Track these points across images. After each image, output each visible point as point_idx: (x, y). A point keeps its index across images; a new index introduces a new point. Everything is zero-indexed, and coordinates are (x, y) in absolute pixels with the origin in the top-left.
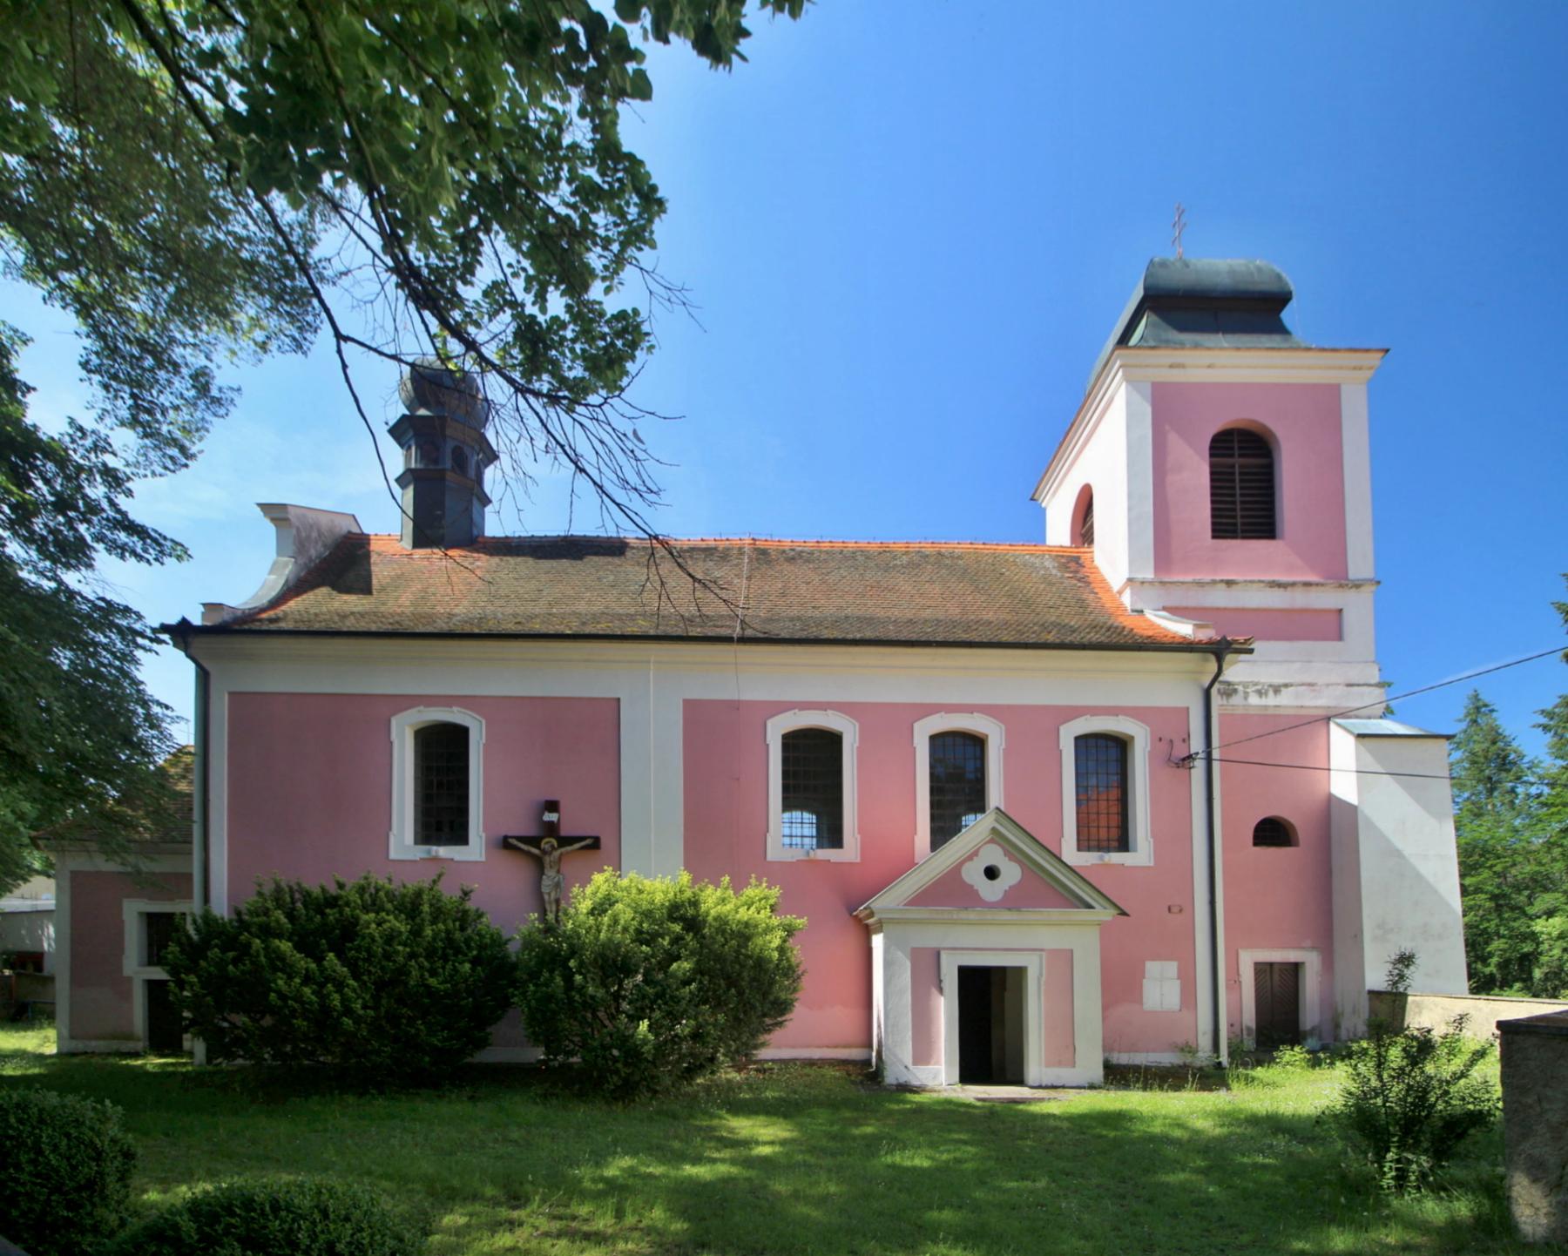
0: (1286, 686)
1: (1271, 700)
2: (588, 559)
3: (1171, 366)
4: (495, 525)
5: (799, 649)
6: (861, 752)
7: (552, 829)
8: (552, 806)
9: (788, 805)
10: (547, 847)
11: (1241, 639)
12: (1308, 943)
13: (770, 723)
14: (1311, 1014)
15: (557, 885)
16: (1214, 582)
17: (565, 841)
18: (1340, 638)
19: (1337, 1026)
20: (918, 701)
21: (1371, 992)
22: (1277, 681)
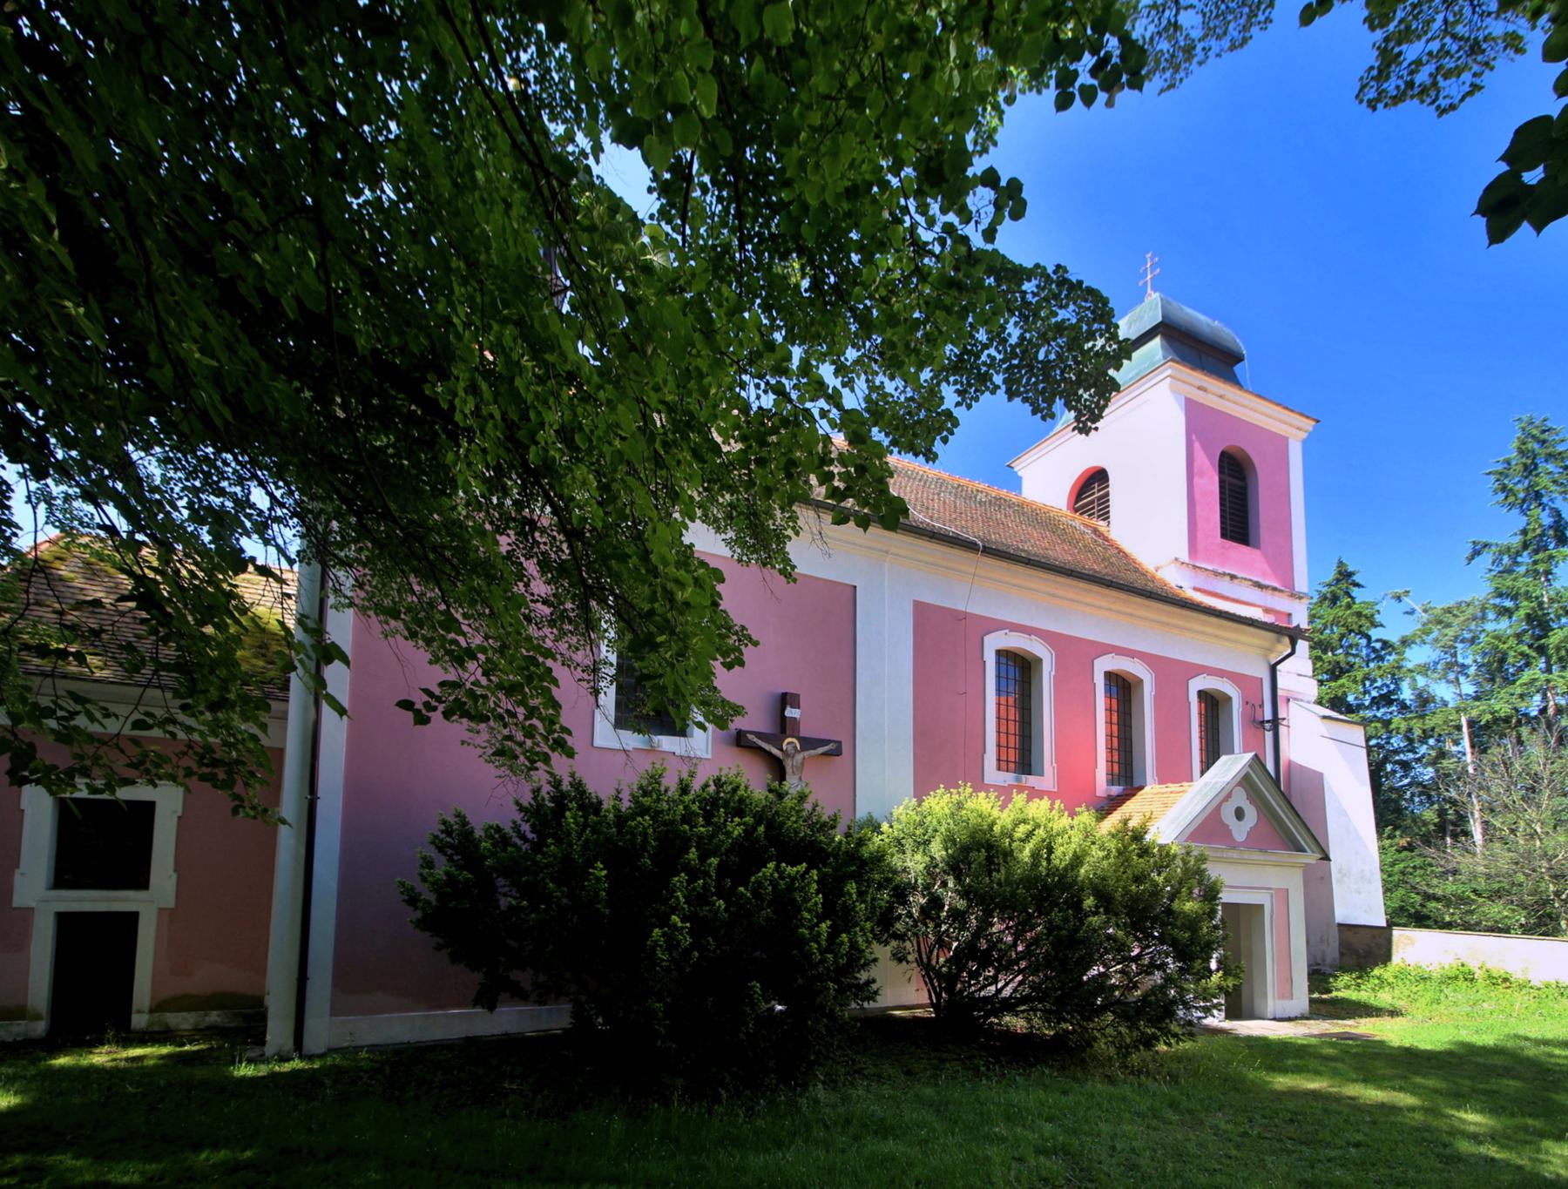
3: (1199, 388)
4: (1157, 342)
5: (1020, 568)
16: (1224, 574)
17: (808, 744)
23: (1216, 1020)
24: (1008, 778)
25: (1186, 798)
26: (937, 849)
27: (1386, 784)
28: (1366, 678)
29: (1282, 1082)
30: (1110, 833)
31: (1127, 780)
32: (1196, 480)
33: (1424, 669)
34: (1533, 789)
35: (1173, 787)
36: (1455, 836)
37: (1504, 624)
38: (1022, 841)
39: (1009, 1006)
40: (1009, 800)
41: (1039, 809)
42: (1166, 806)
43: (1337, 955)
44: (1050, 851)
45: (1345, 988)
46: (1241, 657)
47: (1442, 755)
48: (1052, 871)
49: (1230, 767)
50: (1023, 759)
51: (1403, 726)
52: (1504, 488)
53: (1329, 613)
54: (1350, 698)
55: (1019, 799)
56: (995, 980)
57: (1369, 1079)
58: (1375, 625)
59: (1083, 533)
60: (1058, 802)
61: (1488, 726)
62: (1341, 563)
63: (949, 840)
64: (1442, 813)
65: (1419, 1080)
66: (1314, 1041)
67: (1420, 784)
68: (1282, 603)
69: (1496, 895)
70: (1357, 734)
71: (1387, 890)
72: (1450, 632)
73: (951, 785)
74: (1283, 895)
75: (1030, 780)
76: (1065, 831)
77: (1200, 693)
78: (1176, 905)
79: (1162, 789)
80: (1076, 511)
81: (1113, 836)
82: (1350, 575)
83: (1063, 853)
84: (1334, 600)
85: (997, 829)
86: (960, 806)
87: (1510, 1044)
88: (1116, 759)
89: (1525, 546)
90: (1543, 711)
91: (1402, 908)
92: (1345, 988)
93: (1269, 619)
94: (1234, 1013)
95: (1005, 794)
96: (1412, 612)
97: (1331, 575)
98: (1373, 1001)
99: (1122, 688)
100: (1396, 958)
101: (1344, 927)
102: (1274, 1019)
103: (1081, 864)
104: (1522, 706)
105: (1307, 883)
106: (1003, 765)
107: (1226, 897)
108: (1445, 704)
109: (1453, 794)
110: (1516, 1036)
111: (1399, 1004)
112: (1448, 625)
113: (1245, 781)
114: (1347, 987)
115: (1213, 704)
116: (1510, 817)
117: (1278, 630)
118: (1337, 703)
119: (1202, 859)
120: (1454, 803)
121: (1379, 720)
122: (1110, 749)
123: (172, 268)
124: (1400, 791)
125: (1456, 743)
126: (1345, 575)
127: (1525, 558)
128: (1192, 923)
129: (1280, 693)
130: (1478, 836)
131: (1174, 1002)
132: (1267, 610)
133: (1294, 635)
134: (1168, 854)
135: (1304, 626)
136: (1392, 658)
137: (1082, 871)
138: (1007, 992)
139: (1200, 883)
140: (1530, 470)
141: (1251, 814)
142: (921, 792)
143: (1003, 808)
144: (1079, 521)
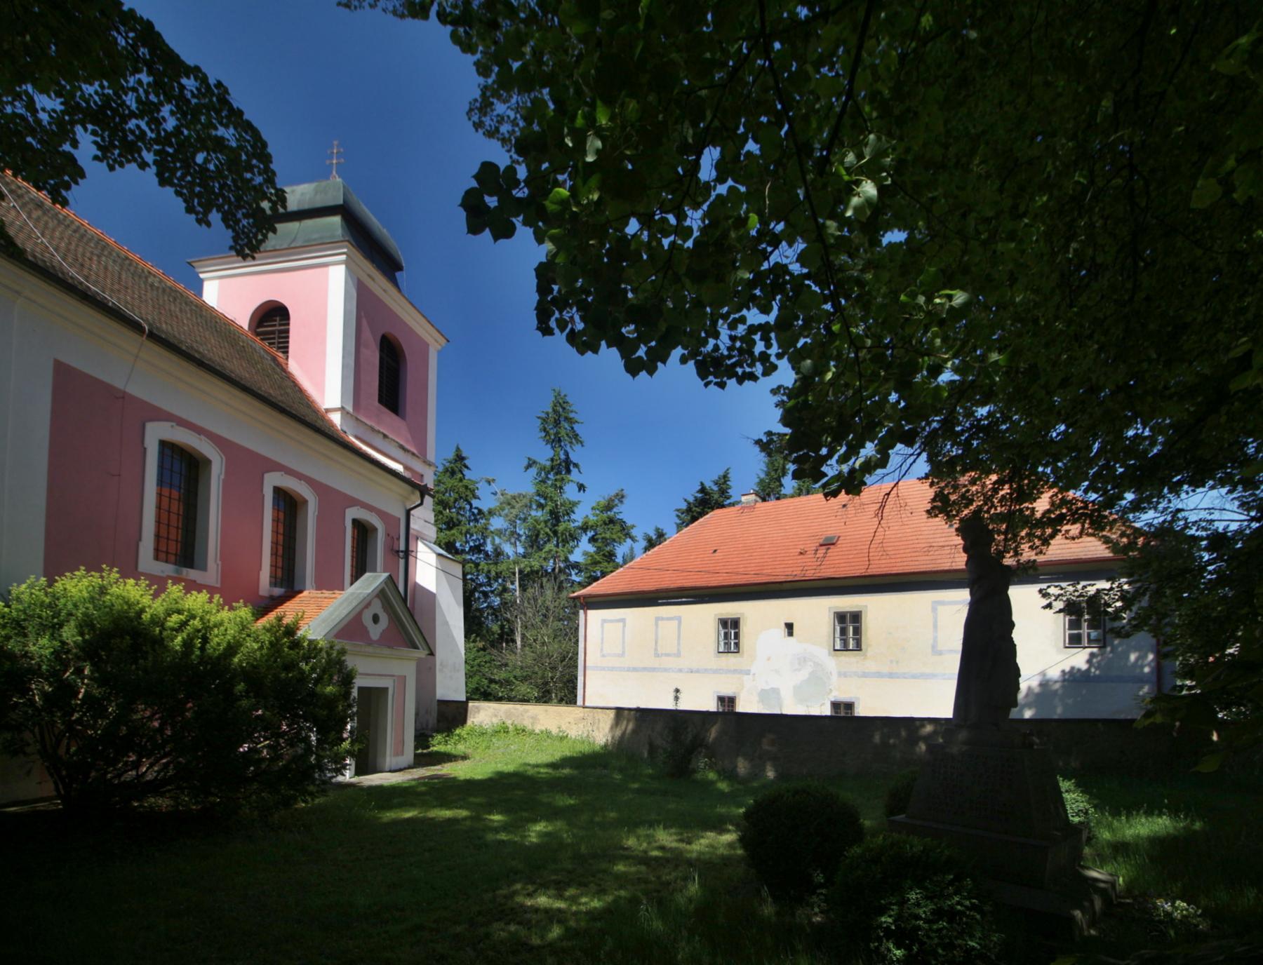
5: (193, 368)
16: (379, 432)
23: (348, 776)
24: (166, 569)
25: (336, 602)
26: (69, 633)
27: (475, 606)
28: (467, 532)
29: (390, 815)
30: (264, 628)
31: (289, 582)
32: (363, 350)
33: (500, 533)
34: (545, 616)
35: (327, 593)
36: (507, 643)
37: (539, 513)
38: (172, 629)
39: (155, 787)
40: (161, 589)
41: (196, 601)
42: (320, 608)
44: (205, 640)
45: (438, 744)
46: (390, 500)
47: (505, 590)
48: (204, 659)
49: (371, 582)
50: (183, 547)
51: (486, 568)
52: (545, 430)
53: (450, 482)
54: (458, 545)
55: (175, 590)
56: (136, 765)
57: (445, 804)
58: (476, 497)
59: (262, 357)
60: (217, 597)
61: (528, 575)
62: (458, 449)
63: (86, 624)
64: (502, 627)
65: (472, 799)
66: (413, 783)
67: (492, 607)
68: (418, 466)
69: (524, 679)
70: (458, 570)
71: (469, 676)
72: (514, 512)
73: (93, 567)
74: (403, 679)
75: (192, 574)
76: (221, 624)
77: (164, 445)
78: (318, 689)
79: (315, 593)
80: (258, 334)
81: (268, 630)
83: (218, 641)
84: (453, 473)
85: (146, 617)
86: (103, 590)
87: (521, 769)
88: (280, 564)
89: (552, 468)
90: (554, 570)
91: (477, 689)
92: (438, 744)
93: (407, 475)
94: (360, 771)
95: (159, 585)
96: (495, 494)
97: (451, 455)
98: (453, 752)
99: (289, 505)
100: (469, 722)
102: (390, 771)
103: (234, 654)
104: (544, 564)
105: (419, 672)
106: (163, 556)
107: (359, 682)
108: (508, 557)
109: (508, 616)
110: (526, 764)
111: (469, 751)
112: (513, 507)
113: (381, 594)
114: (439, 743)
115: (363, 531)
116: (534, 632)
117: (414, 485)
118: (449, 547)
119: (343, 652)
120: (508, 620)
121: (473, 562)
122: (274, 553)
124: (481, 611)
125: (513, 583)
126: (460, 458)
127: (551, 476)
128: (330, 702)
129: (411, 531)
130: (519, 643)
131: (312, 767)
132: (406, 468)
133: (424, 491)
134: (315, 648)
135: (431, 486)
136: (483, 521)
137: (236, 660)
138: (149, 777)
139: (340, 671)
140: (557, 423)
141: (384, 620)
142: (53, 570)
143: (156, 595)
144: (258, 343)
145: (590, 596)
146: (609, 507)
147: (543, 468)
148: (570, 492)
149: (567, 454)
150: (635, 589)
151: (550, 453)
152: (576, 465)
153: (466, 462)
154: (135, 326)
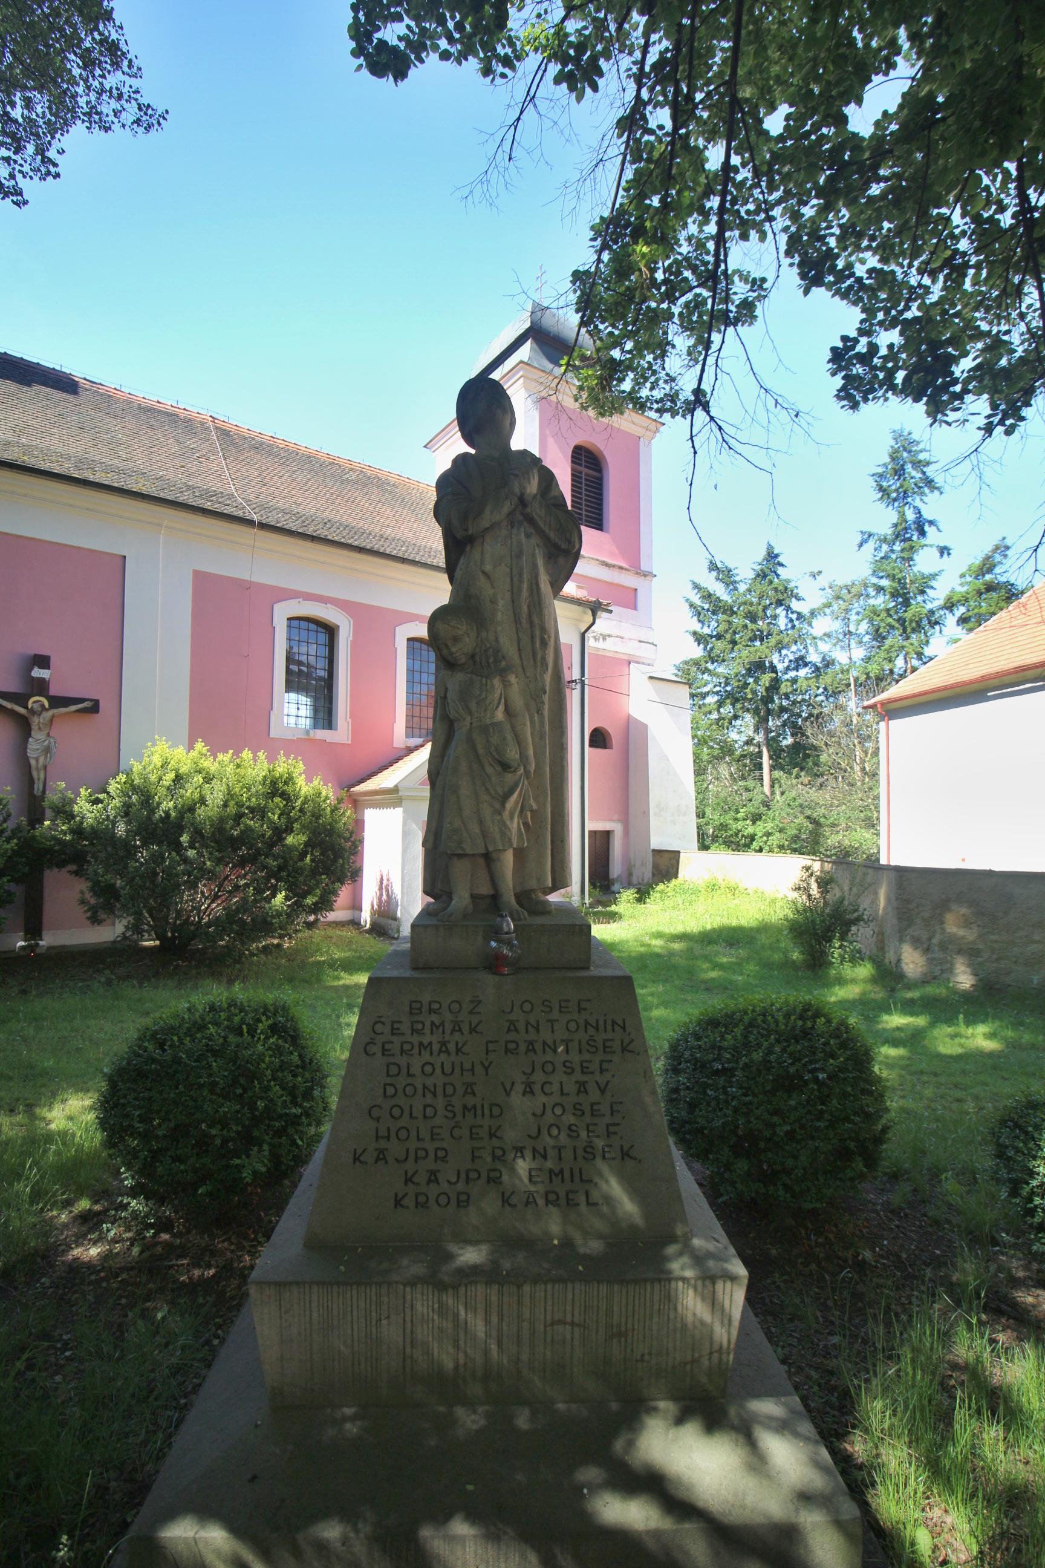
0: (609, 636)
1: (600, 645)
2: (37, 388)
4: (525, 351)
5: (309, 544)
6: (355, 645)
7: (41, 687)
8: (43, 661)
9: (290, 687)
10: (36, 707)
11: (605, 602)
12: (616, 817)
13: (276, 607)
14: (616, 869)
15: (47, 750)
17: (58, 702)
18: (635, 609)
19: (630, 874)
20: (342, 597)
21: (654, 851)
22: (605, 632)
43: (650, 875)
82: (777, 556)
84: (765, 576)
101: (657, 852)
123: (652, 221)
126: (772, 556)
145: (891, 701)
146: (987, 566)
147: (884, 540)
148: (925, 561)
149: (918, 512)
150: (952, 680)
151: (892, 516)
152: (931, 523)
153: (780, 559)
154: (250, 523)
